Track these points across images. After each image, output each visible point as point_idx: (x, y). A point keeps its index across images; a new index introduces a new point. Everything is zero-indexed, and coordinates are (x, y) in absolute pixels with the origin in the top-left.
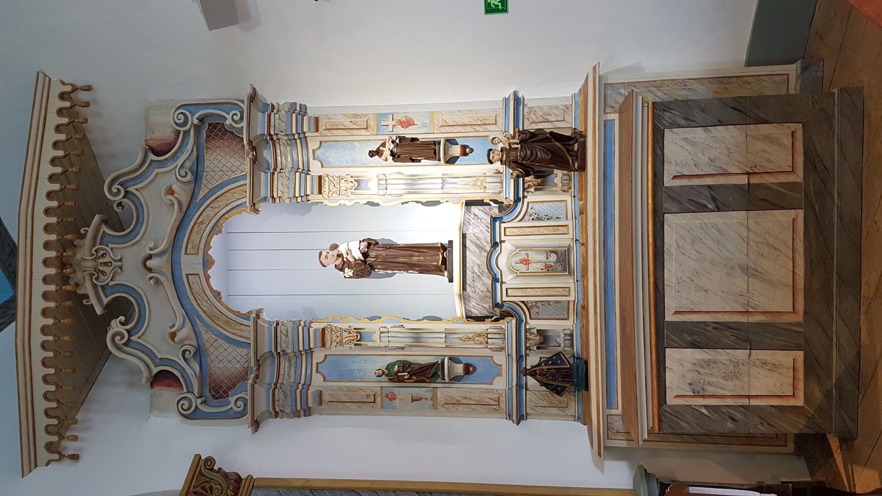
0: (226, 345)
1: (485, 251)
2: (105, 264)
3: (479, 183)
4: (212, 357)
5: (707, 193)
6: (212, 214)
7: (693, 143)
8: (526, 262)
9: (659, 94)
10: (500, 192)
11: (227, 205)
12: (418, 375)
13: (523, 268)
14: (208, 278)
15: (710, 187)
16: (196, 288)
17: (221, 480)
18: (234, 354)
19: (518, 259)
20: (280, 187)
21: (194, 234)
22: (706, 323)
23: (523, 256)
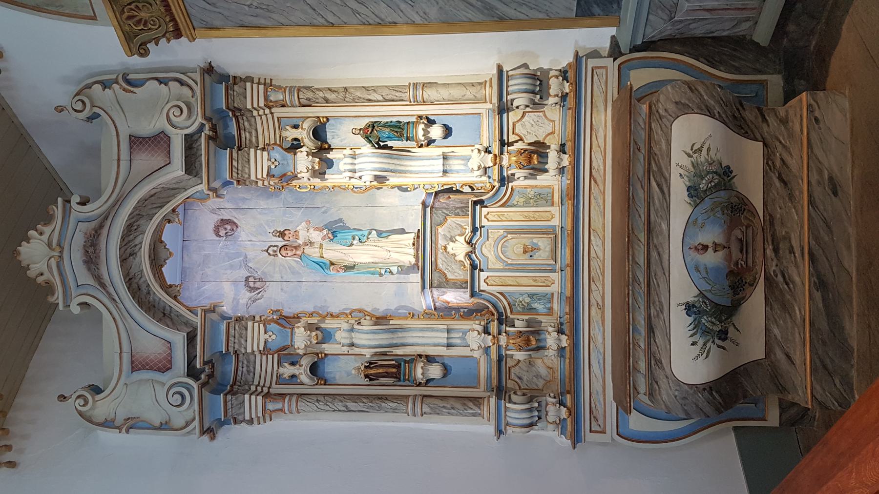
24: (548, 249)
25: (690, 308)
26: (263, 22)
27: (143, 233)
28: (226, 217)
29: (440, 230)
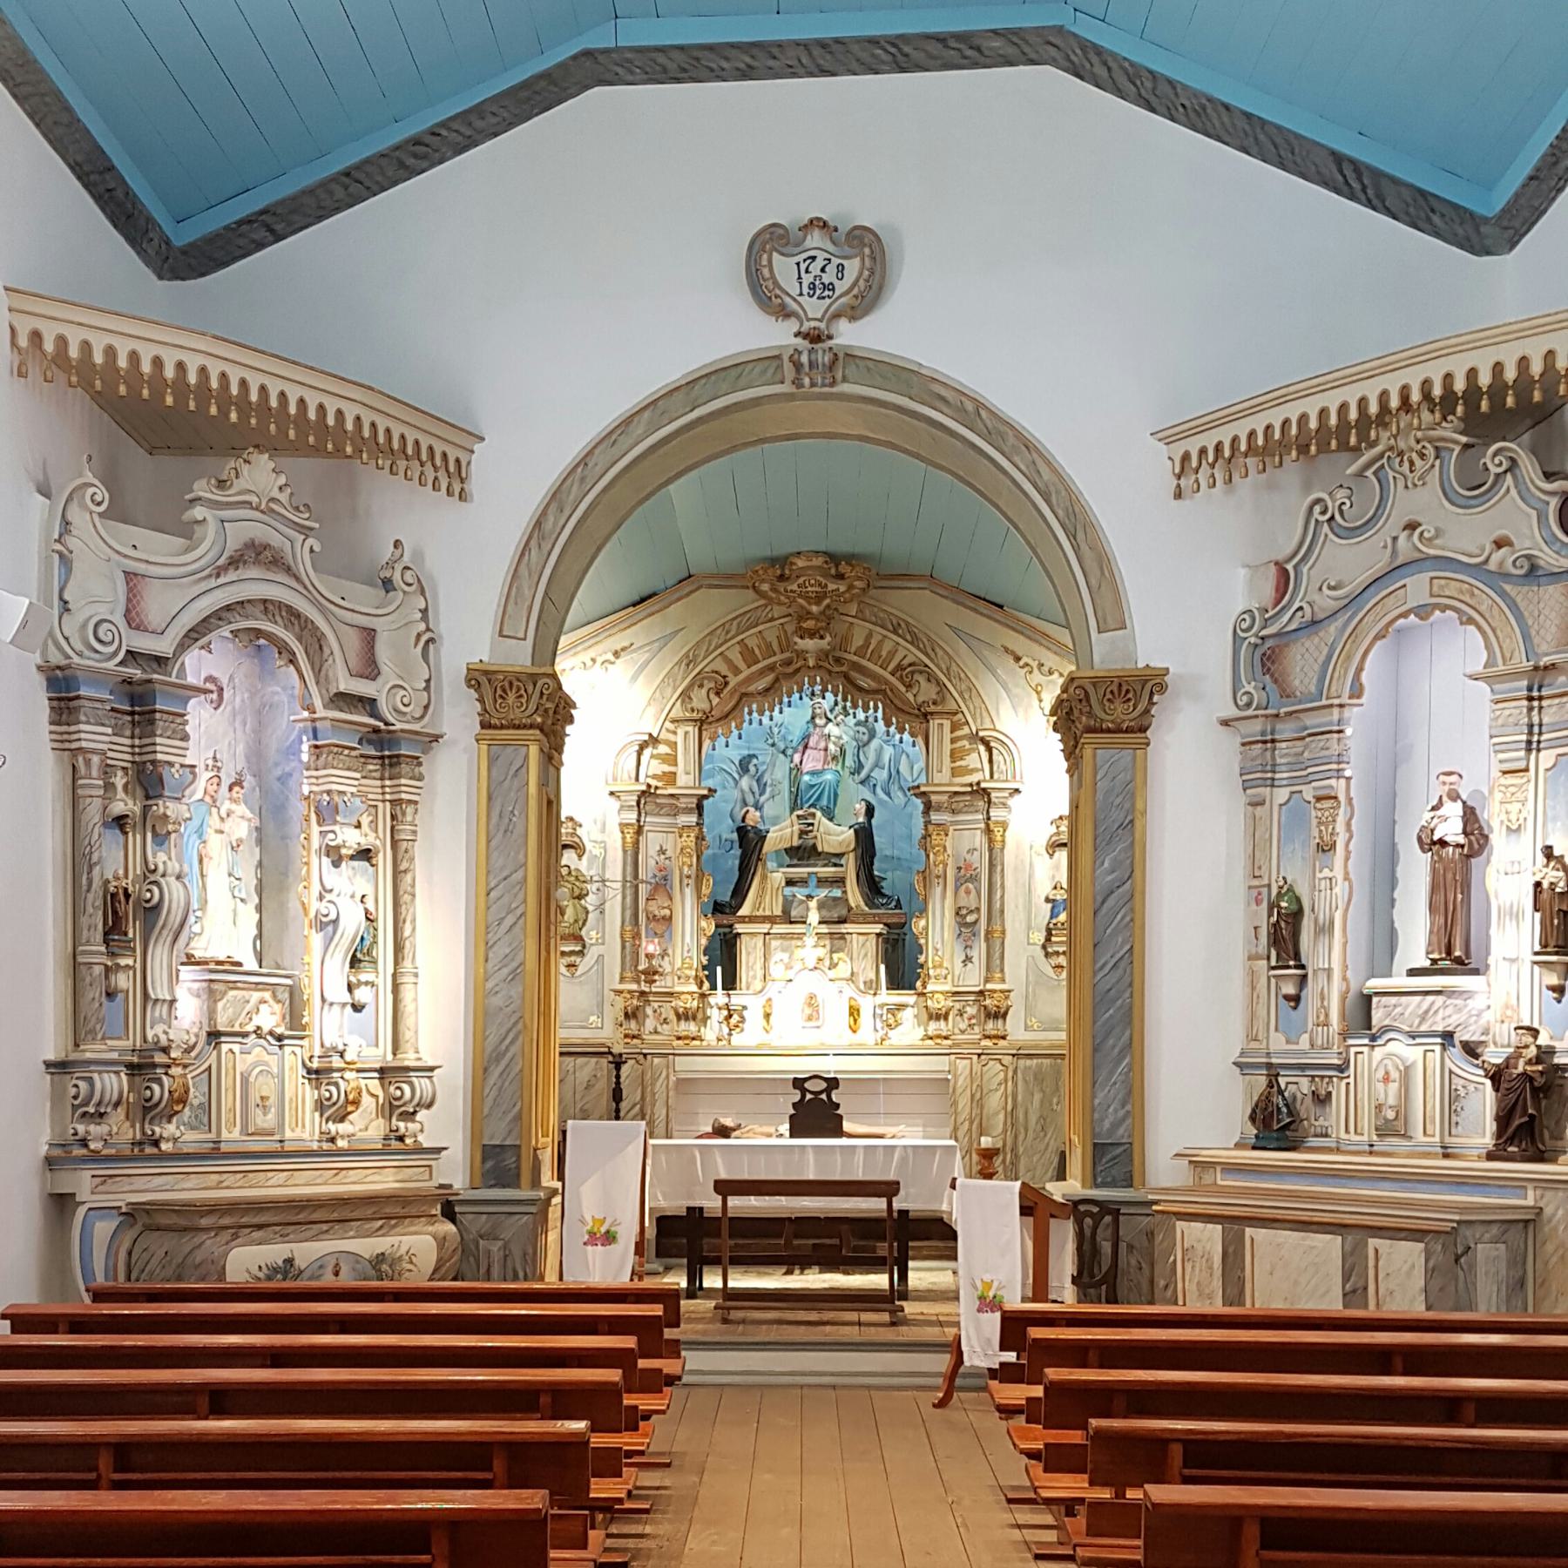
0: (1322, 659)
1: (1420, 1024)
2: (1412, 463)
3: (1509, 1013)
4: (1307, 644)
5: (1360, 1284)
6: (1483, 608)
7: (1409, 1274)
8: (1386, 1079)
9: (1554, 1259)
10: (1495, 1044)
11: (1494, 630)
12: (1285, 933)
13: (1380, 1074)
14: (1404, 615)
15: (1366, 1289)
16: (1391, 600)
17: (1141, 708)
18: (1311, 674)
19: (1390, 1068)
20: (1507, 712)
21: (1458, 584)
22: (1243, 1269)
23: (1394, 1075)
24: (265, 1125)
25: (289, 1261)
26: (494, 820)
27: (286, 628)
28: (226, 695)
29: (267, 995)
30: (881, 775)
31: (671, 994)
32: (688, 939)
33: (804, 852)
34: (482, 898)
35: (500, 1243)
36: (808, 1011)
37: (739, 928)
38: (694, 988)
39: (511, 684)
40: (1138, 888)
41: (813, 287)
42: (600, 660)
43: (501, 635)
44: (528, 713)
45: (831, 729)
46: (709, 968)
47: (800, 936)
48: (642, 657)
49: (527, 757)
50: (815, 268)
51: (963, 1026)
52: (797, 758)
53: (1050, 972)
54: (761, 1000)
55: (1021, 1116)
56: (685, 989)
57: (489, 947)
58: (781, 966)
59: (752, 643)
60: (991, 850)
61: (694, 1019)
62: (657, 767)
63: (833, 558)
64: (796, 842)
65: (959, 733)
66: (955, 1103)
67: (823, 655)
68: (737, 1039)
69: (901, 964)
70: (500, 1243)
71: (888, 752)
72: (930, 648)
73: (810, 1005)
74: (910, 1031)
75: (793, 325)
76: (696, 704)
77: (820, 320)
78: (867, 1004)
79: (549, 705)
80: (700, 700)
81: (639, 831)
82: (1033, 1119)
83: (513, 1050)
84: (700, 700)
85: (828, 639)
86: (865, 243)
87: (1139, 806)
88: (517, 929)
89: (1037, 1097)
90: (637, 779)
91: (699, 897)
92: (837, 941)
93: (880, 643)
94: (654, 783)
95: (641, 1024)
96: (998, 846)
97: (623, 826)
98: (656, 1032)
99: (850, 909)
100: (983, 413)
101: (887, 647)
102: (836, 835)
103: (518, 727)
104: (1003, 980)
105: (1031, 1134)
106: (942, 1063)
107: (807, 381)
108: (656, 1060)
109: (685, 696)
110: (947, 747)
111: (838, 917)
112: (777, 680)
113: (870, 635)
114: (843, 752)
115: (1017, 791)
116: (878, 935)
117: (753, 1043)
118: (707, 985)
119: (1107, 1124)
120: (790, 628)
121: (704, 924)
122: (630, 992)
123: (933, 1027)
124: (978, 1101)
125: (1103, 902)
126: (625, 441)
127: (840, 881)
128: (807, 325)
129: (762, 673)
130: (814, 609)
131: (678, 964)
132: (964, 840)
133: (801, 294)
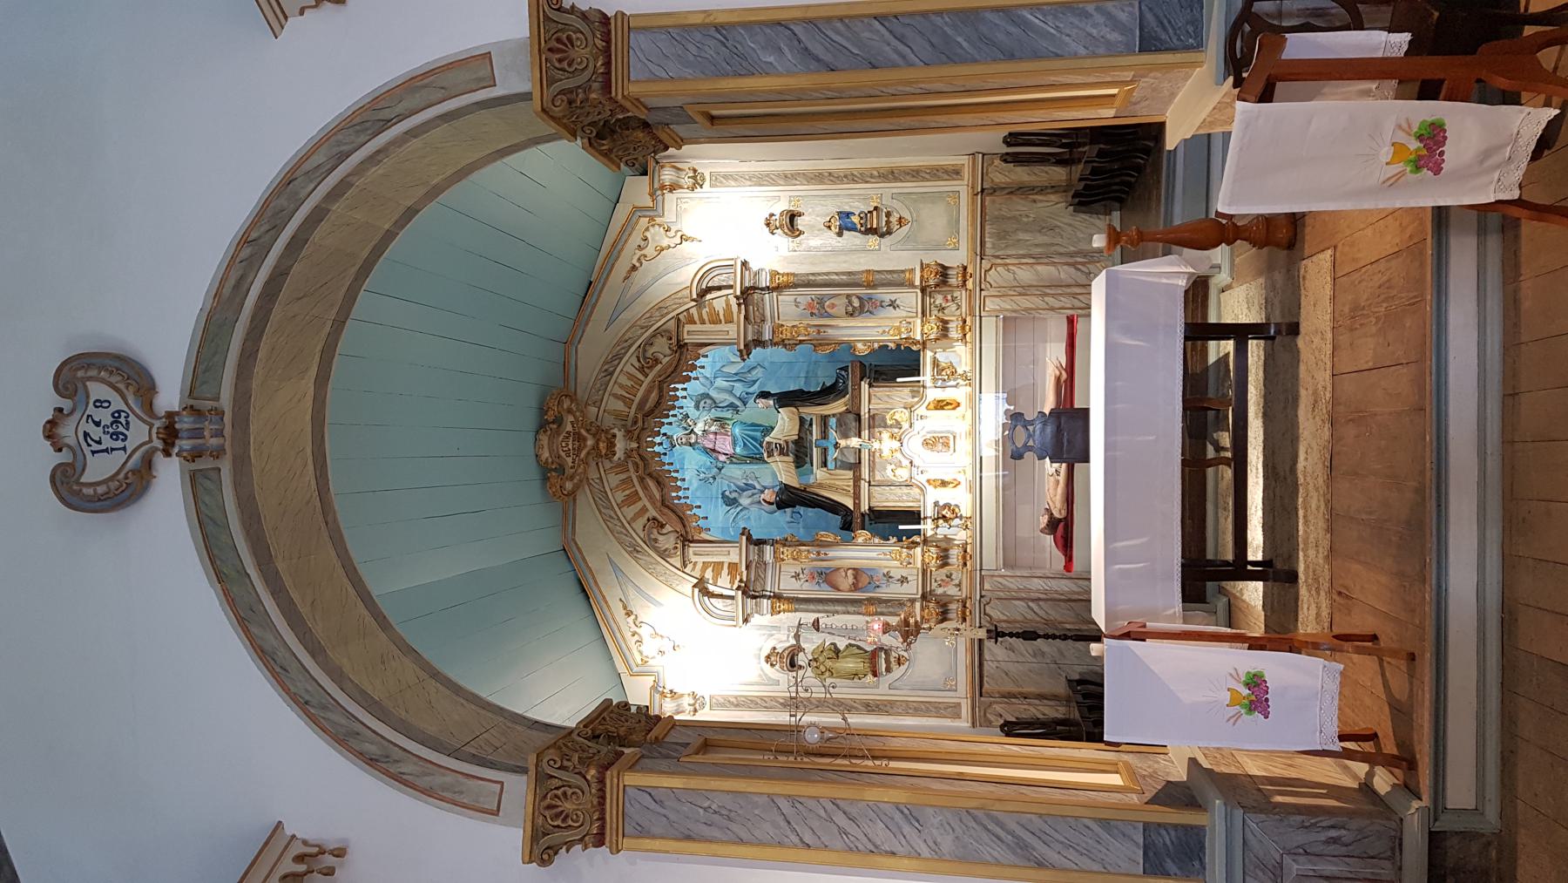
17: (580, 24)
26: (717, 834)
30: (739, 388)
31: (924, 572)
32: (874, 555)
33: (799, 452)
34: (811, 854)
35: (1287, 860)
36: (940, 447)
37: (865, 508)
38: (918, 550)
39: (549, 807)
40: (798, 14)
41: (115, 436)
42: (634, 628)
43: (496, 813)
44: (586, 788)
45: (698, 429)
46: (900, 536)
47: (872, 454)
48: (632, 593)
49: (639, 788)
50: (96, 432)
51: (954, 307)
52: (722, 458)
53: (905, 229)
54: (930, 489)
55: (1039, 250)
56: (919, 558)
57: (876, 850)
58: (899, 471)
59: (620, 496)
60: (796, 286)
61: (946, 550)
62: (724, 580)
63: (542, 426)
64: (791, 458)
65: (696, 317)
66: (1026, 310)
67: (629, 434)
68: (966, 510)
69: (897, 365)
70: (1287, 860)
71: (720, 382)
72: (624, 344)
73: (934, 444)
74: (959, 355)
75: (159, 458)
76: (670, 545)
77: (151, 426)
78: (933, 394)
79: (575, 758)
80: (668, 541)
81: (778, 597)
82: (1041, 239)
83: (1013, 826)
84: (668, 541)
85: (615, 431)
86: (72, 376)
87: (698, 20)
88: (853, 811)
89: (1021, 236)
90: (732, 598)
91: (837, 544)
92: (876, 422)
93: (621, 386)
94: (736, 584)
95: (951, 599)
96: (791, 279)
97: (774, 612)
98: (959, 585)
99: (848, 411)
100: (254, 235)
101: (623, 380)
102: (784, 424)
103: (603, 798)
104: (912, 271)
105: (1058, 240)
106: (990, 326)
107: (214, 441)
108: (987, 586)
109: (664, 554)
110: (708, 327)
111: (854, 421)
112: (650, 475)
113: (616, 396)
114: (717, 420)
115: (744, 264)
116: (870, 386)
117: (969, 497)
118: (916, 538)
119: (1114, 36)
120: (608, 465)
121: (860, 540)
122: (922, 609)
123: (954, 333)
124: (1024, 290)
125: (818, 60)
126: (281, 654)
127: (824, 419)
128: (158, 444)
129: (645, 488)
130: (590, 442)
131: (897, 563)
132: (787, 310)
133: (124, 449)
